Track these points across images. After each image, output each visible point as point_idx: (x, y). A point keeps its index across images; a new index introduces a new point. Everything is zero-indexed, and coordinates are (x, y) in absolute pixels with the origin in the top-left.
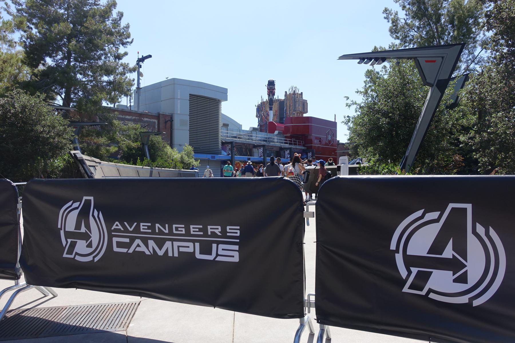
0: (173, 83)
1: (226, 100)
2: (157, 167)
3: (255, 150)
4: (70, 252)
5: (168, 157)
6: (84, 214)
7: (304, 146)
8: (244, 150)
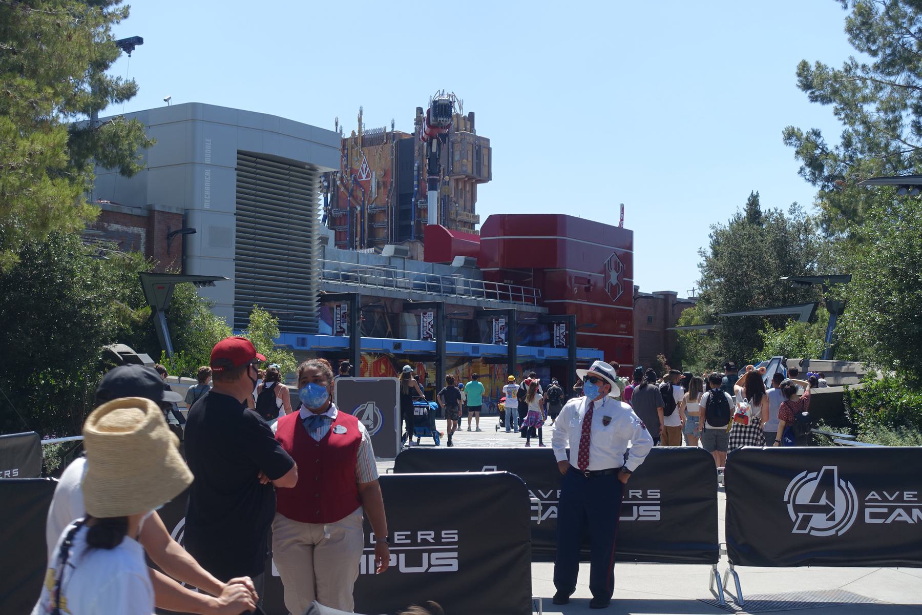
3: (409, 318)
4: (803, 525)
6: (826, 484)
7: (541, 304)
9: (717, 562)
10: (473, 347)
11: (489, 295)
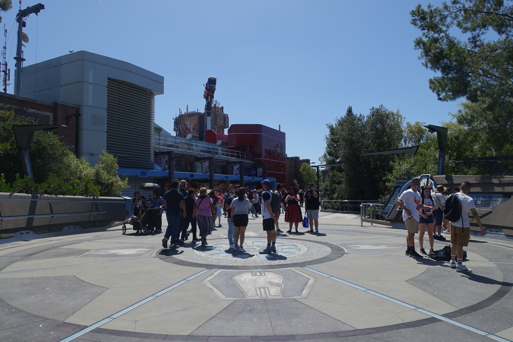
0: (81, 59)
1: (162, 92)
2: (46, 193)
3: (198, 164)
5: (71, 174)
7: (252, 160)
8: (183, 163)
9: (263, 220)
10: (226, 176)
11: (232, 156)
